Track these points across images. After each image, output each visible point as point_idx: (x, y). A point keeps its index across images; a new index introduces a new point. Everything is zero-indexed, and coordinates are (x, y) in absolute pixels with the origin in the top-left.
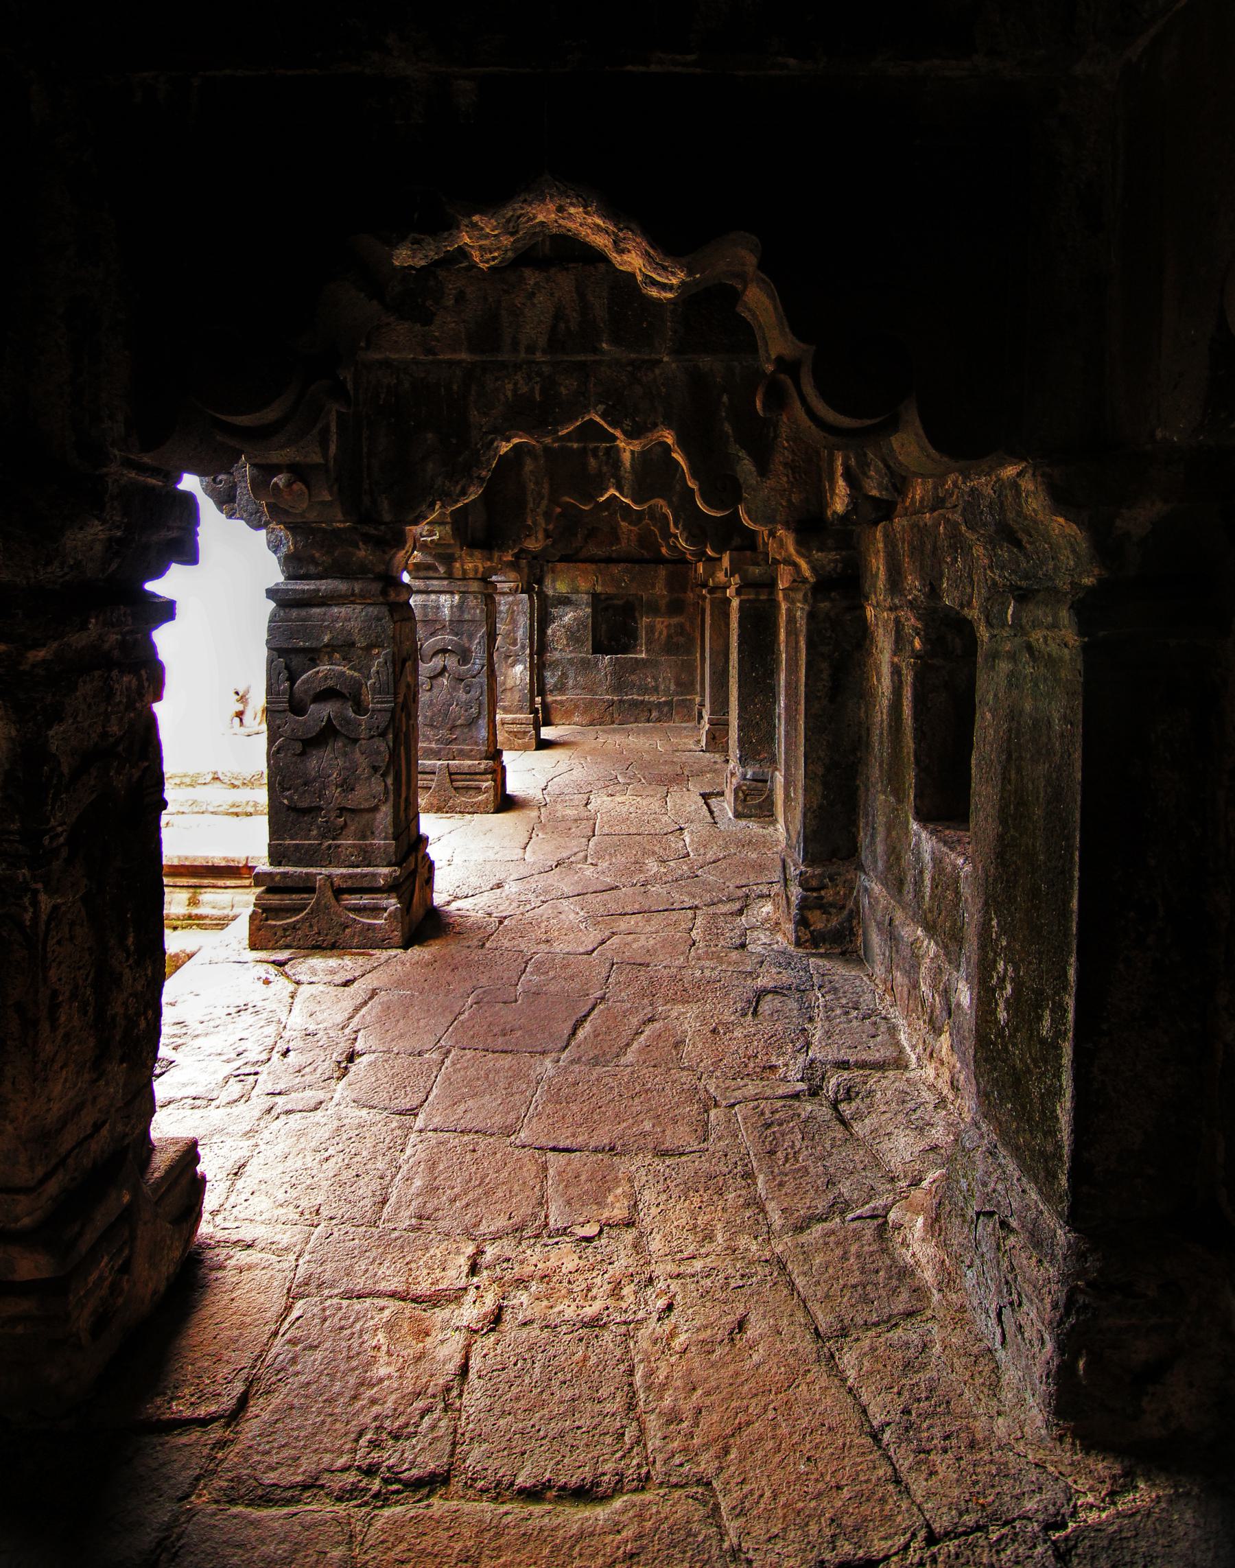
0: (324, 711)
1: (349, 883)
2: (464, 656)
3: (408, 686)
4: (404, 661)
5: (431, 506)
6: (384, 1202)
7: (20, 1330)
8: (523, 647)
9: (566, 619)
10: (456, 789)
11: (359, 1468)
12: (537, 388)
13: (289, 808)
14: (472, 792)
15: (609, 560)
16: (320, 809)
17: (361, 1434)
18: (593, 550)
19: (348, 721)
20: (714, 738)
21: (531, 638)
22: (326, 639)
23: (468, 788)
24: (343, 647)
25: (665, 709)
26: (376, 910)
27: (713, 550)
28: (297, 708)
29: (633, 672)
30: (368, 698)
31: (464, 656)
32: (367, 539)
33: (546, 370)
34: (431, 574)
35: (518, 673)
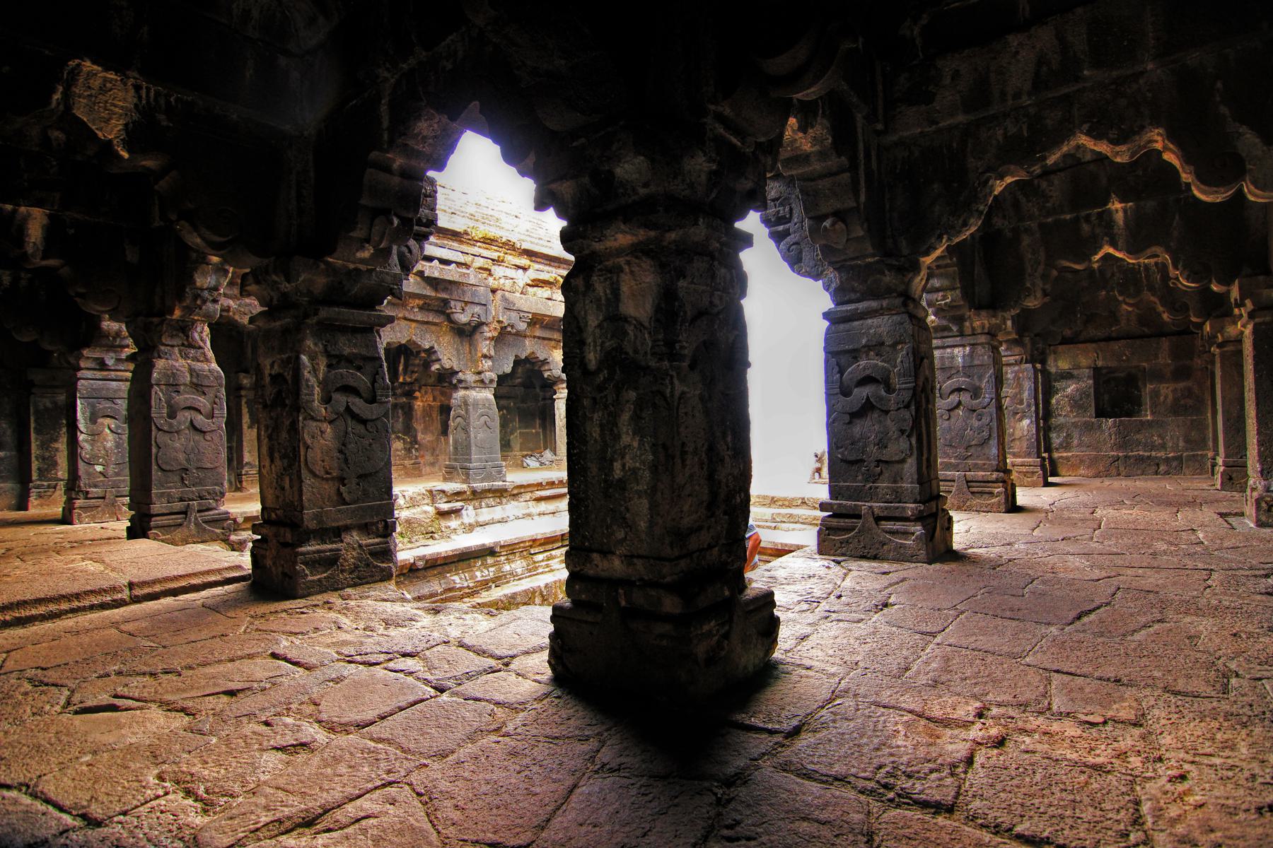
0: (862, 393)
1: (885, 514)
2: (976, 393)
3: (927, 379)
4: (922, 359)
5: (940, 238)
6: (907, 669)
7: (664, 643)
8: (1029, 406)
9: (1069, 390)
10: (973, 493)
11: (878, 782)
12: (1025, 127)
13: (842, 460)
14: (986, 496)
15: (1108, 339)
16: (862, 461)
17: (880, 767)
18: (1092, 332)
19: (881, 399)
20: (1231, 479)
21: (1036, 398)
22: (864, 341)
23: (982, 493)
24: (876, 347)
25: (1174, 464)
26: (906, 534)
27: (1220, 282)
28: (846, 392)
29: (1138, 432)
30: (896, 382)
31: (976, 393)
32: (890, 267)
33: (1032, 111)
34: (946, 334)
35: (1024, 426)
